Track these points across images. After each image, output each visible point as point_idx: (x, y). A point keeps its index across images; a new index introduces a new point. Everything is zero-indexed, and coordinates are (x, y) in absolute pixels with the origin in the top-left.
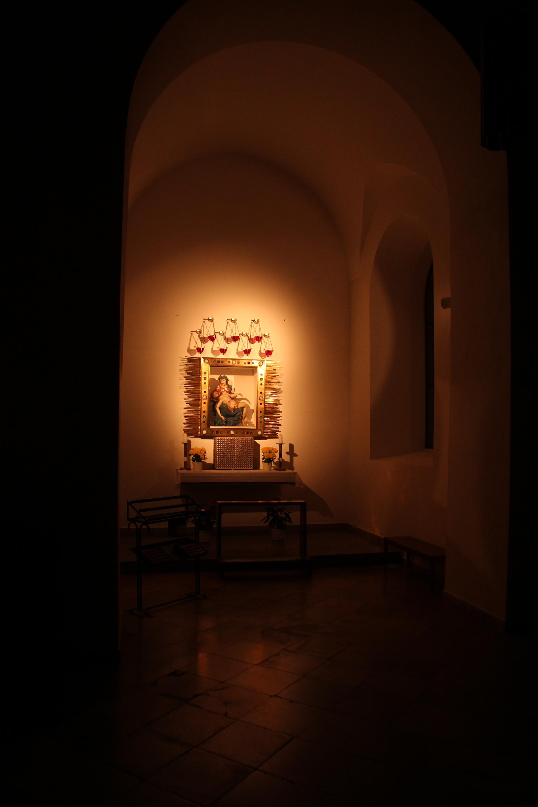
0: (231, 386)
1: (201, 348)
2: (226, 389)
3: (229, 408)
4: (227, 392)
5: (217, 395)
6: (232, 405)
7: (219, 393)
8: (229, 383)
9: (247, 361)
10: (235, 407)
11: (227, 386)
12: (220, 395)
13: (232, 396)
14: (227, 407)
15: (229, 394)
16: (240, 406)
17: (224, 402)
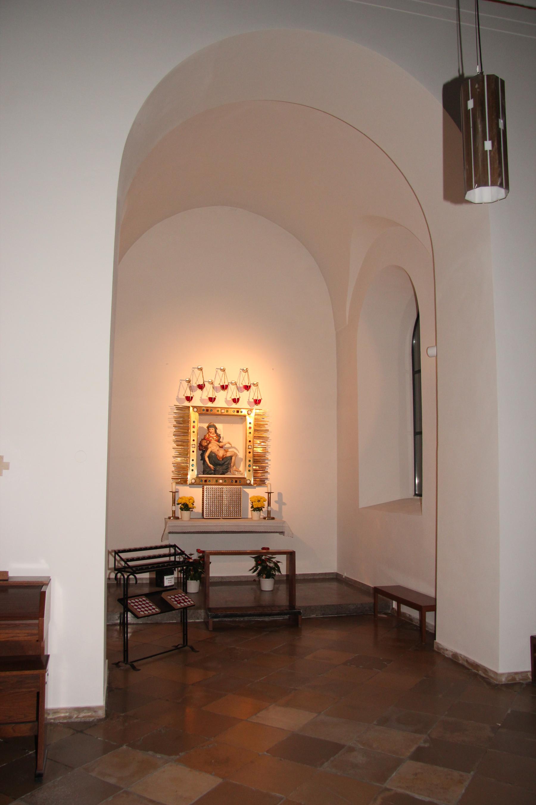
0: (220, 435)
1: (190, 397)
2: (215, 438)
3: (217, 456)
4: (216, 440)
5: (206, 444)
6: (221, 453)
7: (208, 442)
8: (218, 432)
9: (208, 483)
10: (223, 456)
11: (216, 435)
12: (208, 444)
13: (221, 444)
14: (216, 455)
15: (218, 443)
16: (228, 454)
17: (213, 451)
